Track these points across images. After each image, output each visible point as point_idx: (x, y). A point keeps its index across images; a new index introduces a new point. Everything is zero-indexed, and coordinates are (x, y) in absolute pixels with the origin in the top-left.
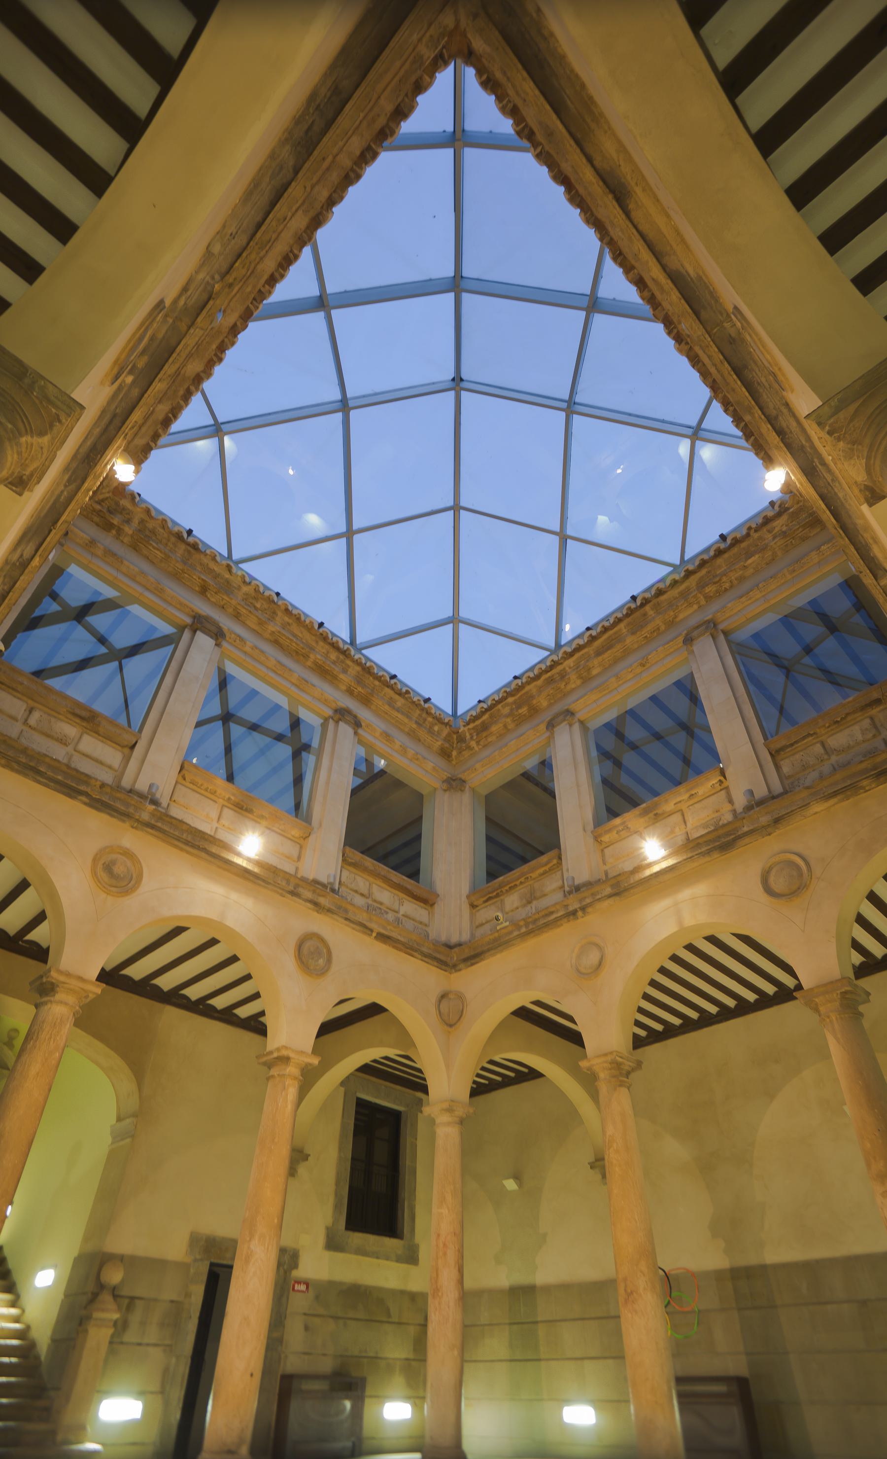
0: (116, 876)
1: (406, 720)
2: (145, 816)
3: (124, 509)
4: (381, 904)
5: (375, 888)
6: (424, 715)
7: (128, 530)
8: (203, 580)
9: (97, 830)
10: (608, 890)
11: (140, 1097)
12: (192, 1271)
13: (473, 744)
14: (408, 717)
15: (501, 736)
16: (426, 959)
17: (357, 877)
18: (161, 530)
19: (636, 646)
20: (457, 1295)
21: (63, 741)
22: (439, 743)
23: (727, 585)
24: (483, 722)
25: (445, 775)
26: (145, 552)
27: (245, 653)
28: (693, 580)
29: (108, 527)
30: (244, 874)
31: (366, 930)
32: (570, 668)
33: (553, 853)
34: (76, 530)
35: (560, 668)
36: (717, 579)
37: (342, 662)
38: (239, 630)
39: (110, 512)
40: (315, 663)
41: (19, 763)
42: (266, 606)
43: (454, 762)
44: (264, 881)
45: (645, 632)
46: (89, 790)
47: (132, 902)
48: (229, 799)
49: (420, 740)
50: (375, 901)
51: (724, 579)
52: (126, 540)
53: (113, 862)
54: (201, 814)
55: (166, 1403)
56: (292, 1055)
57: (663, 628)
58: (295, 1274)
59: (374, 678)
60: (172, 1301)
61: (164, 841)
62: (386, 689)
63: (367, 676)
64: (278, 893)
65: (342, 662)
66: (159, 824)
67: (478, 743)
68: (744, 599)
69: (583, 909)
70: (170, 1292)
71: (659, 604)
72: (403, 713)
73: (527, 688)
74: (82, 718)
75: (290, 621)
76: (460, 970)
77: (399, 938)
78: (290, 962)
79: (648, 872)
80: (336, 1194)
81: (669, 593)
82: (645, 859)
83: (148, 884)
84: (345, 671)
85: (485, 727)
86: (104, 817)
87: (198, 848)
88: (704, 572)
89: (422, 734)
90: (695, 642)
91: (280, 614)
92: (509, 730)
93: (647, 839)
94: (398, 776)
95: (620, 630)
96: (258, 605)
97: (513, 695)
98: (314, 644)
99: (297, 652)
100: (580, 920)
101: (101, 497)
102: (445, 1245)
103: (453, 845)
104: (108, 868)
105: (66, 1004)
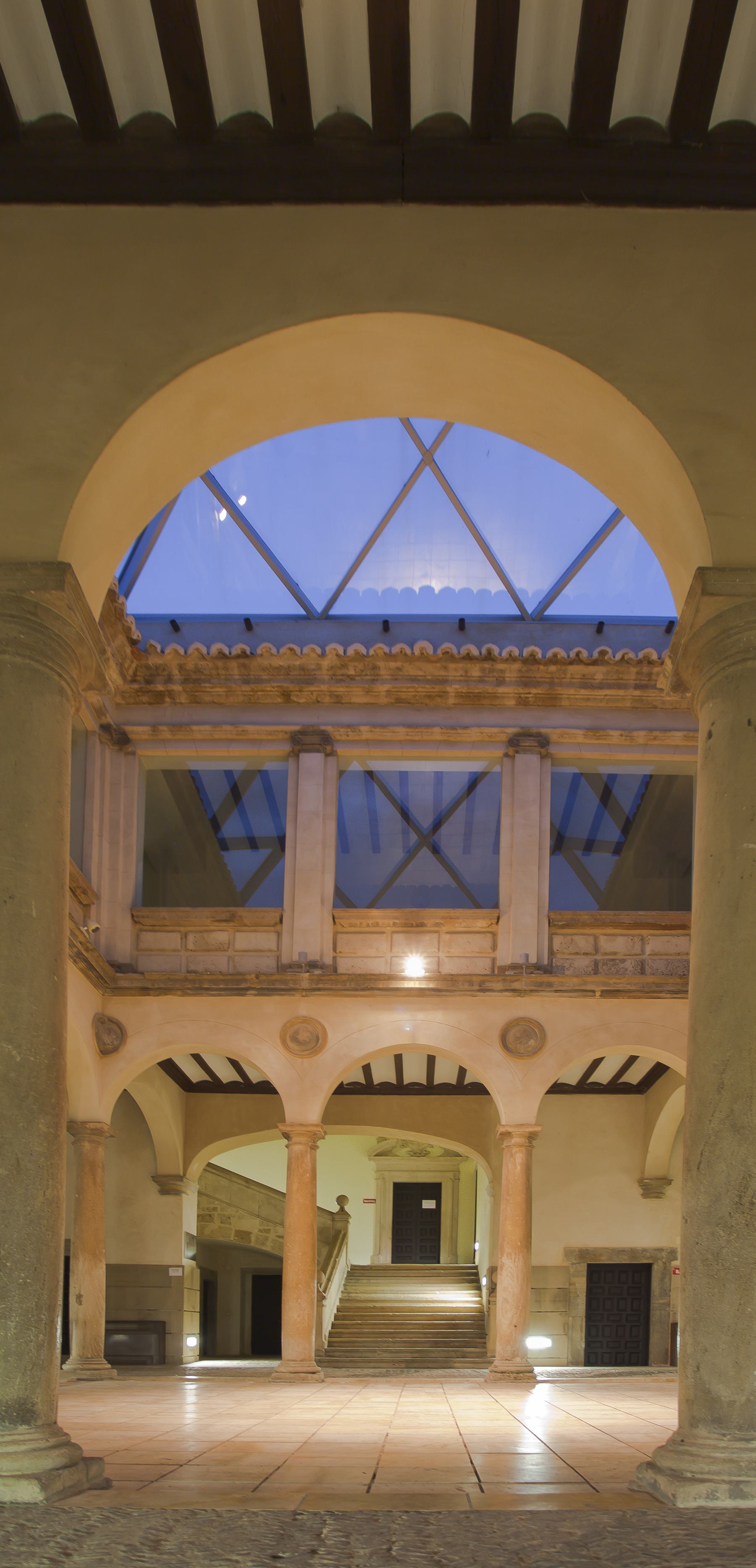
0: (306, 1041)
1: (621, 692)
2: (305, 984)
3: (157, 668)
4: (615, 953)
6: (645, 669)
7: (177, 688)
8: (277, 687)
9: (275, 1011)
14: (619, 687)
16: (678, 996)
17: (576, 938)
18: (203, 663)
26: (207, 699)
27: (367, 742)
29: (158, 698)
30: (420, 992)
31: (585, 993)
34: (135, 728)
37: (492, 671)
38: (347, 717)
39: (148, 682)
40: (459, 695)
41: (189, 989)
42: (360, 666)
44: (447, 991)
46: (248, 985)
47: (326, 1056)
48: (394, 924)
49: (655, 707)
50: (606, 954)
52: (183, 699)
53: (297, 1032)
56: (510, 1130)
65: (492, 671)
66: (321, 986)
70: (556, 1282)
72: (610, 687)
74: (226, 921)
75: (399, 664)
77: (629, 987)
78: (497, 1053)
82: (403, 971)
83: (334, 1038)
84: (501, 682)
86: (276, 998)
87: (372, 989)
91: (381, 664)
96: (351, 672)
98: (443, 673)
99: (429, 697)
101: (131, 672)
104: (295, 1039)
105: (300, 1143)
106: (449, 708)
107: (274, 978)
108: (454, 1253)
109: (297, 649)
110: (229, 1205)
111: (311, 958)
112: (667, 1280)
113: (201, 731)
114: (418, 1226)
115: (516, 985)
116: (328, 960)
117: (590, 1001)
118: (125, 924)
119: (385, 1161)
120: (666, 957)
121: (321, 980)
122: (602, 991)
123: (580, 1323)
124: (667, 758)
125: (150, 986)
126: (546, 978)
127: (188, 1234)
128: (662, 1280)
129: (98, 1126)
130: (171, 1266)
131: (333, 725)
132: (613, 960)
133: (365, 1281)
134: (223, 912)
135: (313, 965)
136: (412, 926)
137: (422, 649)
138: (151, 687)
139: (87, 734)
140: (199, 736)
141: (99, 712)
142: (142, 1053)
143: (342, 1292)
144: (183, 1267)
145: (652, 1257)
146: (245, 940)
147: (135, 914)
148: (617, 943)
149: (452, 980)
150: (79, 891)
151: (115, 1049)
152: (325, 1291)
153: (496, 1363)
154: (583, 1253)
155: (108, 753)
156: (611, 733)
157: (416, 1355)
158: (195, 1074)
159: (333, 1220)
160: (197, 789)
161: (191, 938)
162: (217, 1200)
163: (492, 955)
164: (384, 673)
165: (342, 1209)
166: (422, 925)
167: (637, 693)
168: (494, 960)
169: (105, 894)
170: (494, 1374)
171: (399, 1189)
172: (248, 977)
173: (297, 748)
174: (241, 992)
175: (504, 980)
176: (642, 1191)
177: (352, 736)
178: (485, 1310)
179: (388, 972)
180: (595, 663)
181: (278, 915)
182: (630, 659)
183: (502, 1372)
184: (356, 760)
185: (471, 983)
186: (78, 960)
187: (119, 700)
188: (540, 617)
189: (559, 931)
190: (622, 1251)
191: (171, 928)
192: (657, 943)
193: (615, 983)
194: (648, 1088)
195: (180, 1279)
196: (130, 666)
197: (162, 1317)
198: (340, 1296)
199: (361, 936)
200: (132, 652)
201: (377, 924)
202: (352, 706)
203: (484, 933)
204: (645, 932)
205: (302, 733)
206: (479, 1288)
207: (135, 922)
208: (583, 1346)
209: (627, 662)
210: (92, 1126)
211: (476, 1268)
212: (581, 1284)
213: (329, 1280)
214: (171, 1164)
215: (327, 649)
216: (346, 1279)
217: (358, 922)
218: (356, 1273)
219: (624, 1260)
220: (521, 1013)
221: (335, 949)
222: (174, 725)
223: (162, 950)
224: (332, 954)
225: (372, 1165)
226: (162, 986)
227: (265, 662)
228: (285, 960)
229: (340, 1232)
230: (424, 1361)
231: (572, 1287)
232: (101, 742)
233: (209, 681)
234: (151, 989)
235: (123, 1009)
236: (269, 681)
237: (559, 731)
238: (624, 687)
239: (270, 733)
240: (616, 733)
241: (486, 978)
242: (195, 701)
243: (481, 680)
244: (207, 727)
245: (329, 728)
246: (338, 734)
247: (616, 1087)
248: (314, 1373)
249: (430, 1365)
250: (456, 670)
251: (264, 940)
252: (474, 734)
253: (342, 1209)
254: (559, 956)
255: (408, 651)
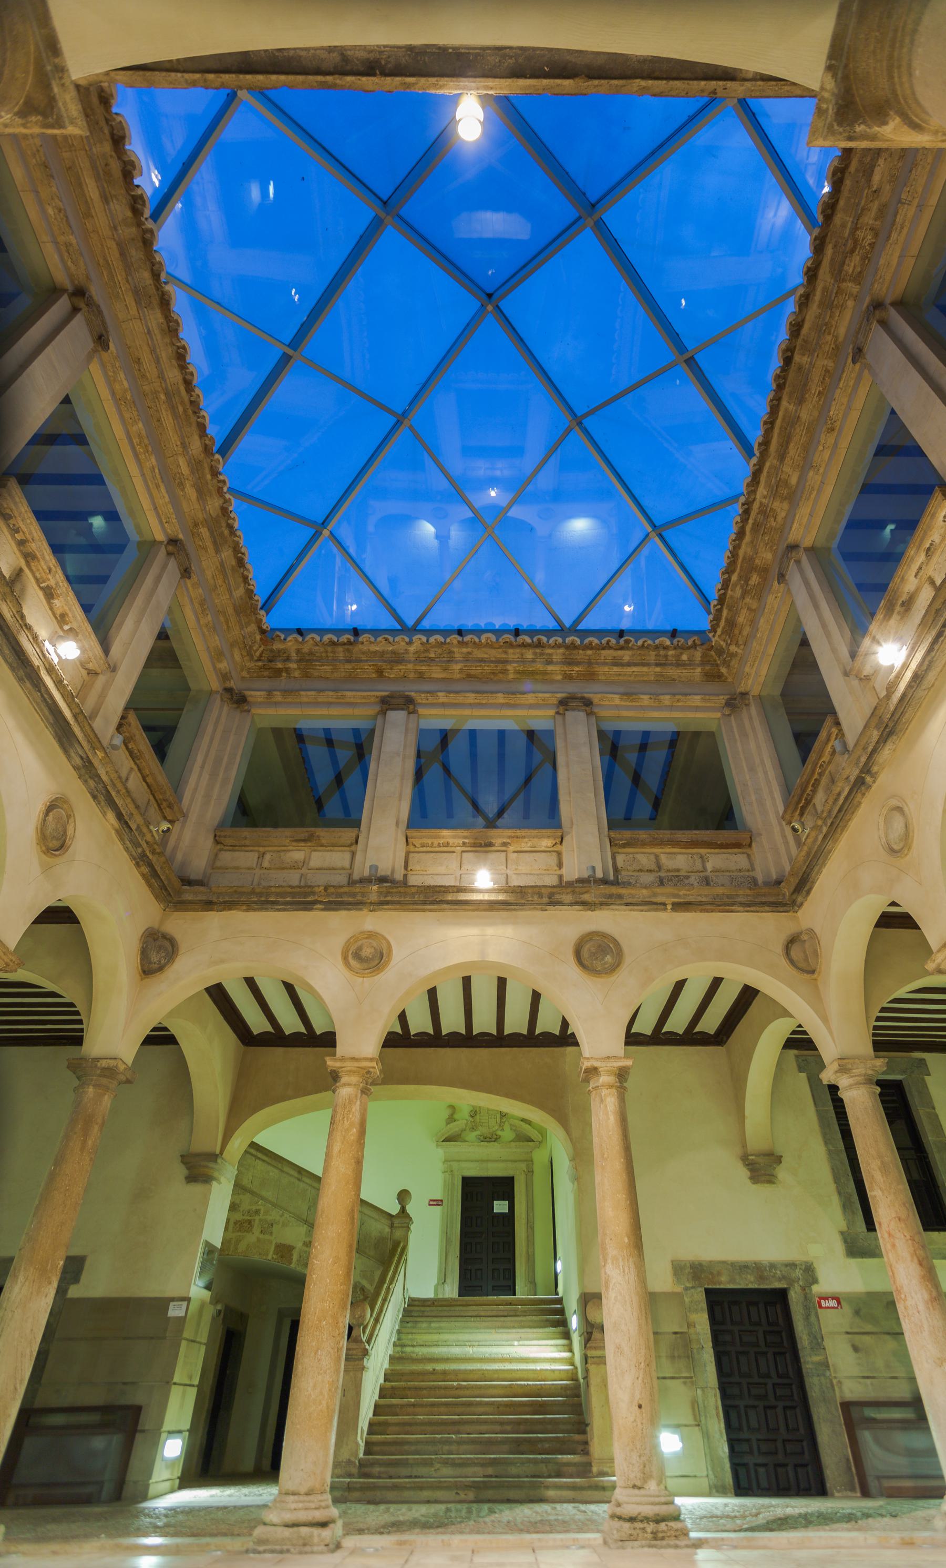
0: (368, 958)
1: (645, 669)
2: (374, 897)
3: (279, 651)
4: (678, 870)
5: (664, 859)
6: (662, 653)
7: (293, 666)
9: (340, 926)
10: (876, 734)
11: (571, 1140)
12: (687, 1300)
13: (733, 648)
14: (643, 665)
15: (753, 623)
16: (752, 909)
17: (637, 856)
19: (816, 414)
20: (926, 1296)
21: (295, 866)
22: (699, 670)
23: (869, 238)
24: (727, 620)
25: (722, 699)
26: (316, 674)
27: (443, 705)
28: (824, 274)
29: (278, 673)
30: (491, 906)
32: (765, 497)
33: (829, 721)
34: (253, 693)
35: (756, 506)
36: (850, 244)
38: (426, 687)
39: (270, 661)
40: (517, 672)
41: (255, 903)
42: (440, 651)
43: (730, 680)
44: (517, 904)
45: (815, 387)
46: (316, 898)
47: (388, 975)
48: (464, 843)
49: (674, 680)
50: (668, 871)
51: (860, 234)
53: (360, 948)
54: (436, 870)
55: (706, 1436)
56: (596, 1064)
57: (830, 364)
58: (816, 1289)
59: (583, 650)
60: (676, 1333)
61: (404, 910)
62: (603, 652)
63: (575, 652)
64: (537, 909)
65: (542, 654)
66: (389, 898)
67: (737, 644)
68: (894, 235)
69: (867, 769)
71: (805, 341)
72: (635, 665)
73: (741, 553)
74: (304, 841)
75: (469, 650)
76: (801, 904)
77: (699, 899)
78: (572, 970)
79: (902, 686)
80: (839, 1193)
81: (808, 318)
83: (398, 955)
84: (549, 662)
85: (731, 623)
86: (343, 913)
88: (829, 251)
89: (672, 672)
90: (865, 350)
91: (456, 650)
92: (754, 611)
93: (883, 644)
94: (692, 729)
95: (786, 410)
96: (432, 655)
97: (733, 571)
98: (504, 656)
99: (493, 673)
100: (874, 787)
101: (258, 654)
102: (890, 1235)
103: (754, 770)
104: (357, 956)
105: (349, 1085)
106: (509, 682)
107: (342, 890)
108: (532, 1282)
109: (391, 639)
110: (275, 1205)
111: (381, 873)
112: (813, 1318)
113: (306, 696)
114: (491, 1242)
115: (586, 897)
116: (399, 876)
117: (663, 915)
118: (206, 844)
119: (455, 1148)
120: (728, 874)
121: (389, 892)
122: (673, 904)
123: (713, 1401)
124: (691, 715)
125: (215, 900)
126: (614, 890)
127: (207, 1244)
128: (807, 1317)
129: (112, 1063)
130: (173, 1299)
131: (416, 692)
132: (677, 876)
133: (424, 1325)
134: (302, 832)
135: (382, 880)
136: (481, 846)
137: (488, 639)
138: (272, 665)
139: (154, 543)
140: (305, 700)
141: (225, 677)
142: (188, 977)
143: (395, 1345)
144: (188, 1300)
145: (784, 1277)
146: (319, 858)
147: (218, 834)
148: (678, 860)
149: (521, 892)
150: (164, 804)
151: (161, 969)
152: (369, 1342)
153: (619, 1494)
154: (696, 1271)
155: (226, 708)
156: (642, 696)
157: (490, 1471)
158: (257, 1022)
159: (392, 1226)
160: (303, 758)
161: (268, 857)
162: (262, 1198)
163: (559, 872)
164: (458, 656)
165: (403, 1210)
166: (490, 844)
167: (658, 669)
168: (561, 877)
169: (193, 817)
170: (617, 1524)
171: (468, 1182)
172: (316, 889)
173: (385, 707)
174: (307, 906)
175: (573, 892)
176: (749, 1173)
177: (431, 700)
178: (580, 1375)
179: (457, 884)
180: (622, 648)
181: (354, 835)
182: (649, 645)
183: (632, 1520)
184: (436, 718)
185: (541, 896)
186: (141, 863)
187: (245, 674)
188: (573, 630)
189: (620, 850)
190: (743, 1268)
191: (251, 848)
192: (716, 860)
193: (685, 894)
194: (728, 1038)
195: (181, 1321)
196: (257, 650)
197: (138, 1398)
198: (390, 1352)
199: (432, 855)
200: (261, 639)
201: (448, 843)
202: (432, 680)
203: (550, 852)
204: (703, 851)
205: (391, 697)
206: (567, 1335)
207: (217, 842)
208: (726, 1449)
209: (647, 648)
210: (104, 1063)
211: (560, 1301)
212: (702, 1322)
213: (377, 1320)
214: (206, 1139)
215: (414, 638)
216: (402, 1321)
217: (429, 841)
218: (417, 1310)
219: (749, 1282)
220: (593, 927)
221: (406, 867)
222: (285, 691)
223: (237, 868)
224: (403, 872)
225: (439, 1153)
226: (227, 899)
227: (365, 648)
228: (356, 877)
229: (398, 1243)
230: (500, 1486)
231: (692, 1330)
232: (222, 700)
233: (319, 661)
234: (216, 903)
235: (181, 925)
236: (367, 661)
237: (599, 696)
238: (648, 665)
239: (364, 697)
240: (646, 697)
241: (555, 890)
242: (306, 675)
243: (533, 661)
244: (313, 693)
245: (413, 694)
246: (420, 698)
247: (691, 1037)
248: (324, 1525)
249: (512, 1494)
250: (514, 654)
251: (339, 858)
252: (530, 699)
253: (403, 1210)
254: (623, 873)
255: (477, 640)
